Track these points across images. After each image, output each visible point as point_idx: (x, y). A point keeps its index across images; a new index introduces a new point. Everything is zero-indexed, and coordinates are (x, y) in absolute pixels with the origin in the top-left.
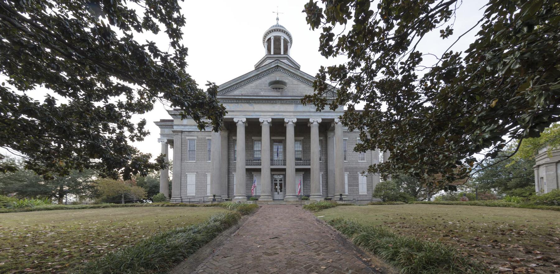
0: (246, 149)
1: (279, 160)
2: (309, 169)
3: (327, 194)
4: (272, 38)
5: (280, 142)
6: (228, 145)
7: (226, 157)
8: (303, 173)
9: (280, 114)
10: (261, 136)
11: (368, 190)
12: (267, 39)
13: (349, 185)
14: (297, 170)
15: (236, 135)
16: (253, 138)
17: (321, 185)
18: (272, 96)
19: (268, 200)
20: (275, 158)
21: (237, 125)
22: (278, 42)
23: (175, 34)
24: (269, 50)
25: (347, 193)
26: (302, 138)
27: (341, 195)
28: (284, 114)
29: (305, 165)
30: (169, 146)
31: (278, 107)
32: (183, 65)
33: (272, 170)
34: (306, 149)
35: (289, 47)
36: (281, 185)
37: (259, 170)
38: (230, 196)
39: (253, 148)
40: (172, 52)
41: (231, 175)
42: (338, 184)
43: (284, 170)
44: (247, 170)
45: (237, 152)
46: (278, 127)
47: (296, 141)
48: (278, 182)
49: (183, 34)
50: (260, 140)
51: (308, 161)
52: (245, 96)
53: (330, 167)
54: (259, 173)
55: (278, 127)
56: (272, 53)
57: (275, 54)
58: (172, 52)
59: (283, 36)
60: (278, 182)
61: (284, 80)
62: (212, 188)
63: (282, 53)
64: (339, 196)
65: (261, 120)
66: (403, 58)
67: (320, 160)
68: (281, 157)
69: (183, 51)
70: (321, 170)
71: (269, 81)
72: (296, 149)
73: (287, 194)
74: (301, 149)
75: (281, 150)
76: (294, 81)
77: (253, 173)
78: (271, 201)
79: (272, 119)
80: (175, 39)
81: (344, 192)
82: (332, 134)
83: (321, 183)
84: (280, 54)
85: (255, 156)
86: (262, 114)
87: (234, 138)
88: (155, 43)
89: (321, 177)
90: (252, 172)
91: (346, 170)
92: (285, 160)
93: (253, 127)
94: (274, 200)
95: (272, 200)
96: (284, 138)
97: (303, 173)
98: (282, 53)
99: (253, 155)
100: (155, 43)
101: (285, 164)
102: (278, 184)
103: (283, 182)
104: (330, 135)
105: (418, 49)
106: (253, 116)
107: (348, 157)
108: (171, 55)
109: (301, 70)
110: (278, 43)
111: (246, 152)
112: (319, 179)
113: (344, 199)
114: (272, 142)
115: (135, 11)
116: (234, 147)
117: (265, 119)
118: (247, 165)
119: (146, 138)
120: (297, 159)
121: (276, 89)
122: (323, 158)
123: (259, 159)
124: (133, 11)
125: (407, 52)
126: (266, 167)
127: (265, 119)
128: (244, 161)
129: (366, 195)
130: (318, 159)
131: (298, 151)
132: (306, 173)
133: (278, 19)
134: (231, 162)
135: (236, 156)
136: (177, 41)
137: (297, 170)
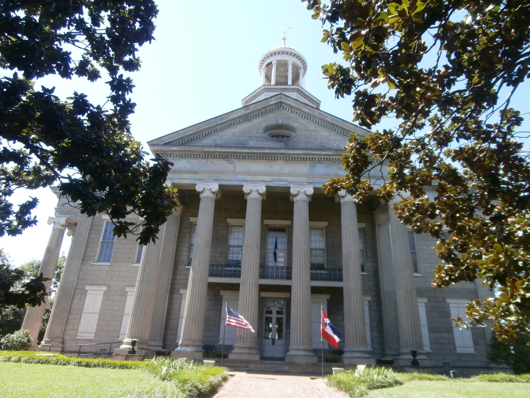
0: (213, 243)
1: (277, 268)
2: (340, 290)
3: (383, 349)
4: (274, 63)
5: (281, 230)
6: (180, 232)
7: (170, 258)
8: (328, 297)
9: (283, 178)
10: (244, 217)
11: (476, 342)
12: (266, 63)
13: (431, 330)
14: (315, 290)
15: (196, 215)
16: (229, 221)
17: (368, 328)
18: (269, 148)
19: (250, 358)
20: (271, 263)
21: (202, 196)
22: (284, 70)
23: (120, 87)
24: (268, 78)
25: (427, 348)
26: (325, 224)
27: (414, 353)
28: (290, 179)
29: (330, 279)
30: (67, 231)
31: (279, 167)
32: (124, 125)
33: (262, 288)
34: (334, 245)
35: (301, 75)
36: (279, 321)
37: (236, 287)
38: (168, 343)
39: (226, 239)
40: (109, 108)
41: (176, 296)
42: (405, 324)
43: (288, 289)
44: (211, 286)
45: (194, 248)
46: (277, 203)
47: (311, 228)
48: (274, 316)
49: (131, 92)
50: (242, 226)
51: (337, 273)
52: (221, 146)
53: (385, 286)
54: (234, 293)
55: (277, 203)
56: (273, 82)
57: (277, 83)
58: (109, 108)
59: (291, 60)
60: (274, 316)
61: (292, 124)
62: (134, 323)
63: (290, 82)
64: (410, 357)
65: (246, 189)
66: (490, 117)
67: (363, 269)
68: (281, 260)
69: (128, 108)
70: (365, 293)
71: (264, 125)
72: (313, 246)
73: (292, 346)
74: (322, 245)
75: (283, 245)
76: (309, 125)
77: (222, 293)
78: (256, 362)
79: (267, 187)
80: (120, 93)
81: (421, 346)
82: (383, 217)
83: (367, 321)
84: (286, 83)
85: (231, 257)
86: (249, 178)
87: (192, 219)
88: (86, 96)
89: (367, 308)
90: (217, 294)
91: (420, 293)
92: (289, 268)
93: (231, 201)
94: (263, 358)
95: (257, 358)
96: (288, 223)
97: (328, 297)
98: (290, 82)
99: (227, 254)
100: (86, 96)
101: (289, 277)
102: (274, 320)
103: (284, 316)
104: (380, 217)
105: (514, 105)
106: (231, 181)
107: (421, 266)
108: (107, 111)
109: (321, 109)
110: (283, 69)
111: (212, 247)
112: (363, 312)
113: (421, 364)
114: (266, 230)
115: (70, 53)
116: (190, 237)
117: (255, 190)
118: (211, 275)
119: (28, 231)
120: (314, 267)
121: (277, 136)
122: (369, 265)
123: (238, 264)
124: (67, 54)
125: (496, 107)
126: (249, 281)
127: (255, 190)
128: (207, 266)
129: (473, 355)
130: (359, 268)
131: (316, 249)
132: (335, 301)
133: (284, 39)
134: (181, 267)
135: (193, 255)
136: (123, 95)
137: (315, 290)
